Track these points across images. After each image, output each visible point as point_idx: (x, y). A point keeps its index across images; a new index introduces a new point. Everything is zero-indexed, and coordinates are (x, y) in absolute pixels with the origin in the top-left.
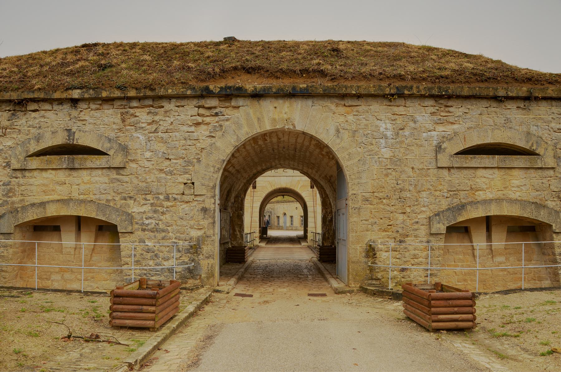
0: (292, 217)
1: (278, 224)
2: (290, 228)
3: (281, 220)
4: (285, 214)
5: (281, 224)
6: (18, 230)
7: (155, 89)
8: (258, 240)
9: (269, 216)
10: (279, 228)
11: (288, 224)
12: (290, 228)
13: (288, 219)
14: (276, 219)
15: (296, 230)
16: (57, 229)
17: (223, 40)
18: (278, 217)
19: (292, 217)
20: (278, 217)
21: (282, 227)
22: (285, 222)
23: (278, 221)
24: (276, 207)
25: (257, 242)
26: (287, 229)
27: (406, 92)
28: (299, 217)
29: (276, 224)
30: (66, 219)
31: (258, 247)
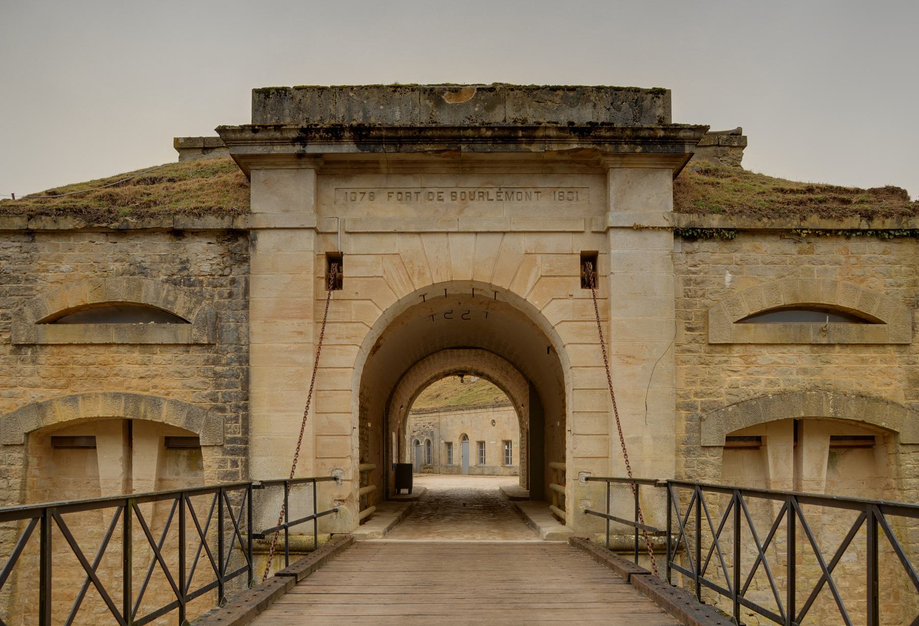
0: (481, 444)
1: (450, 460)
2: (478, 471)
3: (456, 452)
4: (465, 437)
5: (456, 460)
6: (31, 442)
7: (798, 373)
8: (351, 514)
9: (429, 442)
10: (452, 470)
11: (473, 461)
12: (478, 471)
13: (473, 448)
14: (444, 448)
15: (493, 474)
16: (89, 445)
17: (242, 116)
18: (449, 445)
19: (481, 444)
20: (449, 445)
21: (459, 467)
22: (465, 457)
23: (450, 453)
24: (444, 420)
25: (348, 521)
26: (471, 473)
27: (348, 148)
28: (500, 444)
29: (444, 460)
30: (103, 425)
31: (344, 545)
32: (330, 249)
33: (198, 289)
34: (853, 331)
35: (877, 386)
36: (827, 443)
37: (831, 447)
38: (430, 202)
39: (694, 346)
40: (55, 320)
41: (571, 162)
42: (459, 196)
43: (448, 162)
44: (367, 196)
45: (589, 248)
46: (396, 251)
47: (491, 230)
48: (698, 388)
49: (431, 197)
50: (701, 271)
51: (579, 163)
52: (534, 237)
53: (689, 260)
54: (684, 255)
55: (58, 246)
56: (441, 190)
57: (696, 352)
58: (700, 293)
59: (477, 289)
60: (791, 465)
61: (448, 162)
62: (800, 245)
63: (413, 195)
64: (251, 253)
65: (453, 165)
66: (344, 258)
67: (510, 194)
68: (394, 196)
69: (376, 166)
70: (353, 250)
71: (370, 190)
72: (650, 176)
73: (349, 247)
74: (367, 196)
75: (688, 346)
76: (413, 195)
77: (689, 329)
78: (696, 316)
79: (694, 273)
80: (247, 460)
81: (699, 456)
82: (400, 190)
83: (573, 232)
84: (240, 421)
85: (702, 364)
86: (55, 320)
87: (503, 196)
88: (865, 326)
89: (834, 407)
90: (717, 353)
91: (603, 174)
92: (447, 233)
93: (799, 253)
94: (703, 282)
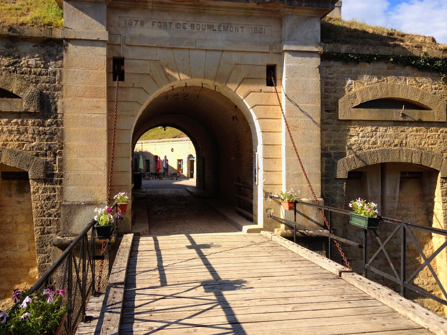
32: (116, 55)
33: (27, 76)
34: (415, 114)
35: (426, 144)
36: (399, 176)
37: (401, 178)
38: (179, 29)
39: (330, 121)
40: (363, 105)
41: (263, 10)
42: (195, 27)
43: (190, 5)
44: (139, 23)
45: (271, 62)
46: (158, 59)
47: (215, 49)
48: (332, 144)
49: (179, 27)
50: (334, 78)
51: (267, 11)
52: (240, 55)
53: (327, 71)
54: (325, 68)
55: (9, 30)
56: (185, 22)
57: (331, 124)
58: (334, 90)
59: (204, 84)
60: (380, 188)
61: (190, 5)
62: (388, 64)
63: (168, 25)
64: (64, 54)
65: (193, 7)
66: (125, 61)
67: (226, 27)
68: (156, 25)
69: (145, 4)
70: (130, 56)
71: (141, 19)
72: (308, 21)
73: (129, 54)
74: (139, 23)
75: (326, 121)
76: (168, 25)
77: (327, 111)
78: (331, 103)
79: (330, 79)
80: (62, 188)
81: (333, 184)
82: (160, 21)
83: (262, 52)
84: (57, 162)
85: (334, 131)
86: (363, 105)
87: (222, 29)
88: (422, 111)
89: (407, 157)
90: (343, 125)
91: (280, 20)
92: (189, 49)
93: (388, 69)
94: (335, 84)
